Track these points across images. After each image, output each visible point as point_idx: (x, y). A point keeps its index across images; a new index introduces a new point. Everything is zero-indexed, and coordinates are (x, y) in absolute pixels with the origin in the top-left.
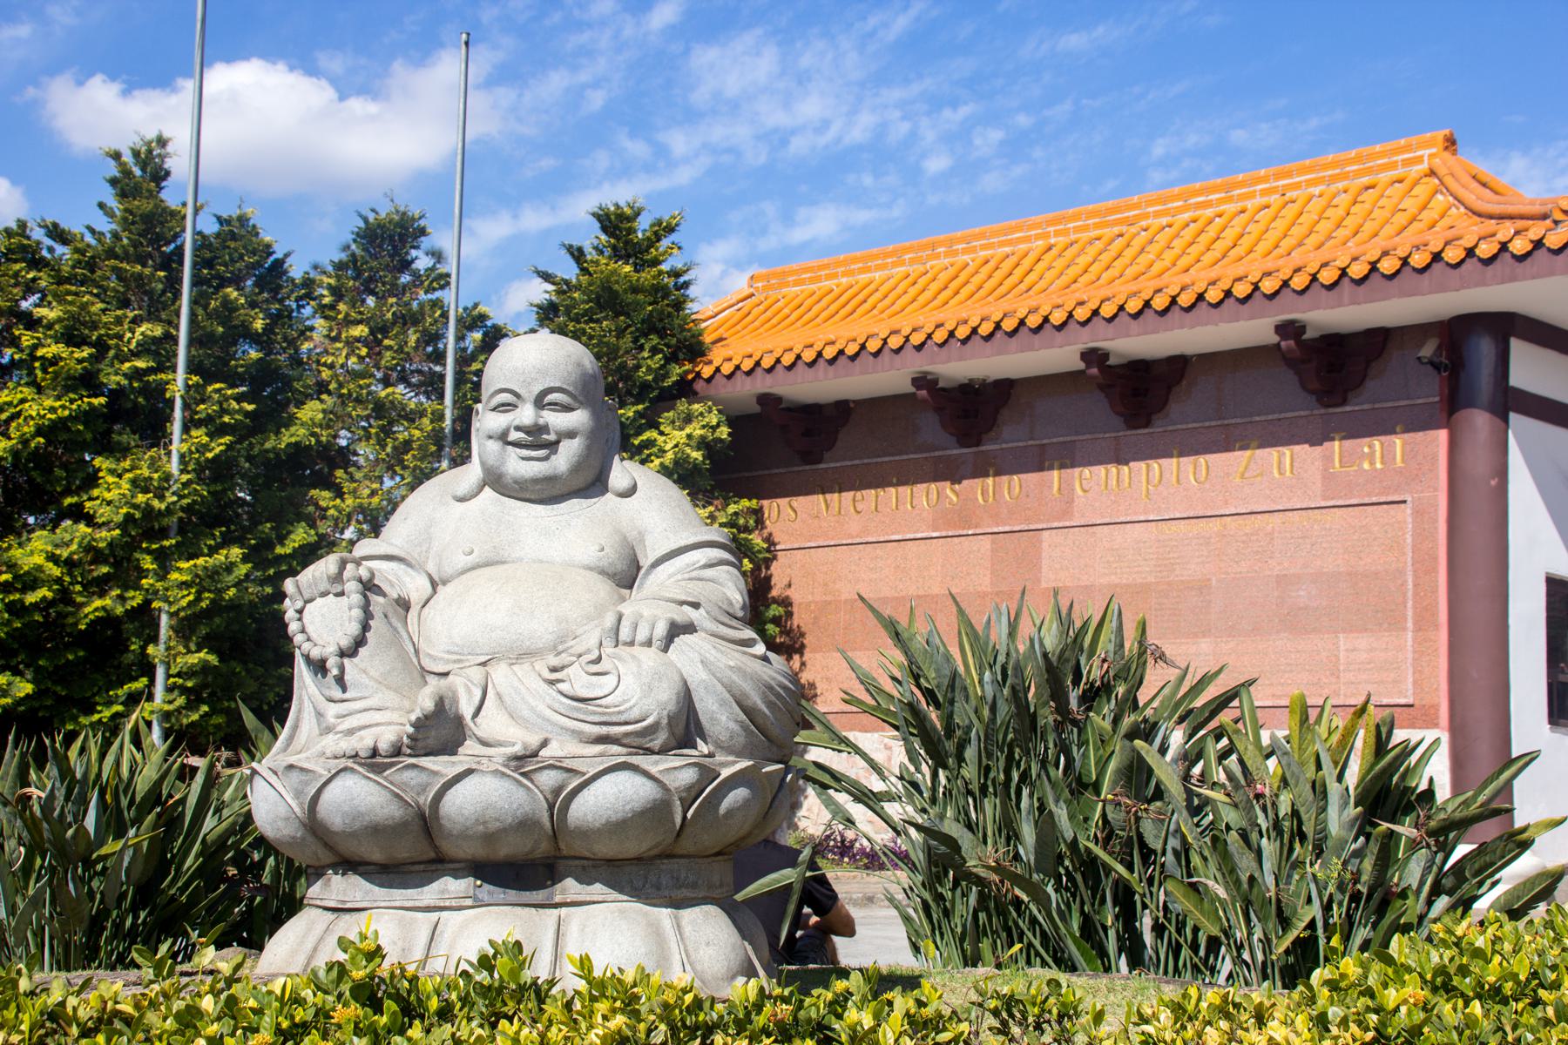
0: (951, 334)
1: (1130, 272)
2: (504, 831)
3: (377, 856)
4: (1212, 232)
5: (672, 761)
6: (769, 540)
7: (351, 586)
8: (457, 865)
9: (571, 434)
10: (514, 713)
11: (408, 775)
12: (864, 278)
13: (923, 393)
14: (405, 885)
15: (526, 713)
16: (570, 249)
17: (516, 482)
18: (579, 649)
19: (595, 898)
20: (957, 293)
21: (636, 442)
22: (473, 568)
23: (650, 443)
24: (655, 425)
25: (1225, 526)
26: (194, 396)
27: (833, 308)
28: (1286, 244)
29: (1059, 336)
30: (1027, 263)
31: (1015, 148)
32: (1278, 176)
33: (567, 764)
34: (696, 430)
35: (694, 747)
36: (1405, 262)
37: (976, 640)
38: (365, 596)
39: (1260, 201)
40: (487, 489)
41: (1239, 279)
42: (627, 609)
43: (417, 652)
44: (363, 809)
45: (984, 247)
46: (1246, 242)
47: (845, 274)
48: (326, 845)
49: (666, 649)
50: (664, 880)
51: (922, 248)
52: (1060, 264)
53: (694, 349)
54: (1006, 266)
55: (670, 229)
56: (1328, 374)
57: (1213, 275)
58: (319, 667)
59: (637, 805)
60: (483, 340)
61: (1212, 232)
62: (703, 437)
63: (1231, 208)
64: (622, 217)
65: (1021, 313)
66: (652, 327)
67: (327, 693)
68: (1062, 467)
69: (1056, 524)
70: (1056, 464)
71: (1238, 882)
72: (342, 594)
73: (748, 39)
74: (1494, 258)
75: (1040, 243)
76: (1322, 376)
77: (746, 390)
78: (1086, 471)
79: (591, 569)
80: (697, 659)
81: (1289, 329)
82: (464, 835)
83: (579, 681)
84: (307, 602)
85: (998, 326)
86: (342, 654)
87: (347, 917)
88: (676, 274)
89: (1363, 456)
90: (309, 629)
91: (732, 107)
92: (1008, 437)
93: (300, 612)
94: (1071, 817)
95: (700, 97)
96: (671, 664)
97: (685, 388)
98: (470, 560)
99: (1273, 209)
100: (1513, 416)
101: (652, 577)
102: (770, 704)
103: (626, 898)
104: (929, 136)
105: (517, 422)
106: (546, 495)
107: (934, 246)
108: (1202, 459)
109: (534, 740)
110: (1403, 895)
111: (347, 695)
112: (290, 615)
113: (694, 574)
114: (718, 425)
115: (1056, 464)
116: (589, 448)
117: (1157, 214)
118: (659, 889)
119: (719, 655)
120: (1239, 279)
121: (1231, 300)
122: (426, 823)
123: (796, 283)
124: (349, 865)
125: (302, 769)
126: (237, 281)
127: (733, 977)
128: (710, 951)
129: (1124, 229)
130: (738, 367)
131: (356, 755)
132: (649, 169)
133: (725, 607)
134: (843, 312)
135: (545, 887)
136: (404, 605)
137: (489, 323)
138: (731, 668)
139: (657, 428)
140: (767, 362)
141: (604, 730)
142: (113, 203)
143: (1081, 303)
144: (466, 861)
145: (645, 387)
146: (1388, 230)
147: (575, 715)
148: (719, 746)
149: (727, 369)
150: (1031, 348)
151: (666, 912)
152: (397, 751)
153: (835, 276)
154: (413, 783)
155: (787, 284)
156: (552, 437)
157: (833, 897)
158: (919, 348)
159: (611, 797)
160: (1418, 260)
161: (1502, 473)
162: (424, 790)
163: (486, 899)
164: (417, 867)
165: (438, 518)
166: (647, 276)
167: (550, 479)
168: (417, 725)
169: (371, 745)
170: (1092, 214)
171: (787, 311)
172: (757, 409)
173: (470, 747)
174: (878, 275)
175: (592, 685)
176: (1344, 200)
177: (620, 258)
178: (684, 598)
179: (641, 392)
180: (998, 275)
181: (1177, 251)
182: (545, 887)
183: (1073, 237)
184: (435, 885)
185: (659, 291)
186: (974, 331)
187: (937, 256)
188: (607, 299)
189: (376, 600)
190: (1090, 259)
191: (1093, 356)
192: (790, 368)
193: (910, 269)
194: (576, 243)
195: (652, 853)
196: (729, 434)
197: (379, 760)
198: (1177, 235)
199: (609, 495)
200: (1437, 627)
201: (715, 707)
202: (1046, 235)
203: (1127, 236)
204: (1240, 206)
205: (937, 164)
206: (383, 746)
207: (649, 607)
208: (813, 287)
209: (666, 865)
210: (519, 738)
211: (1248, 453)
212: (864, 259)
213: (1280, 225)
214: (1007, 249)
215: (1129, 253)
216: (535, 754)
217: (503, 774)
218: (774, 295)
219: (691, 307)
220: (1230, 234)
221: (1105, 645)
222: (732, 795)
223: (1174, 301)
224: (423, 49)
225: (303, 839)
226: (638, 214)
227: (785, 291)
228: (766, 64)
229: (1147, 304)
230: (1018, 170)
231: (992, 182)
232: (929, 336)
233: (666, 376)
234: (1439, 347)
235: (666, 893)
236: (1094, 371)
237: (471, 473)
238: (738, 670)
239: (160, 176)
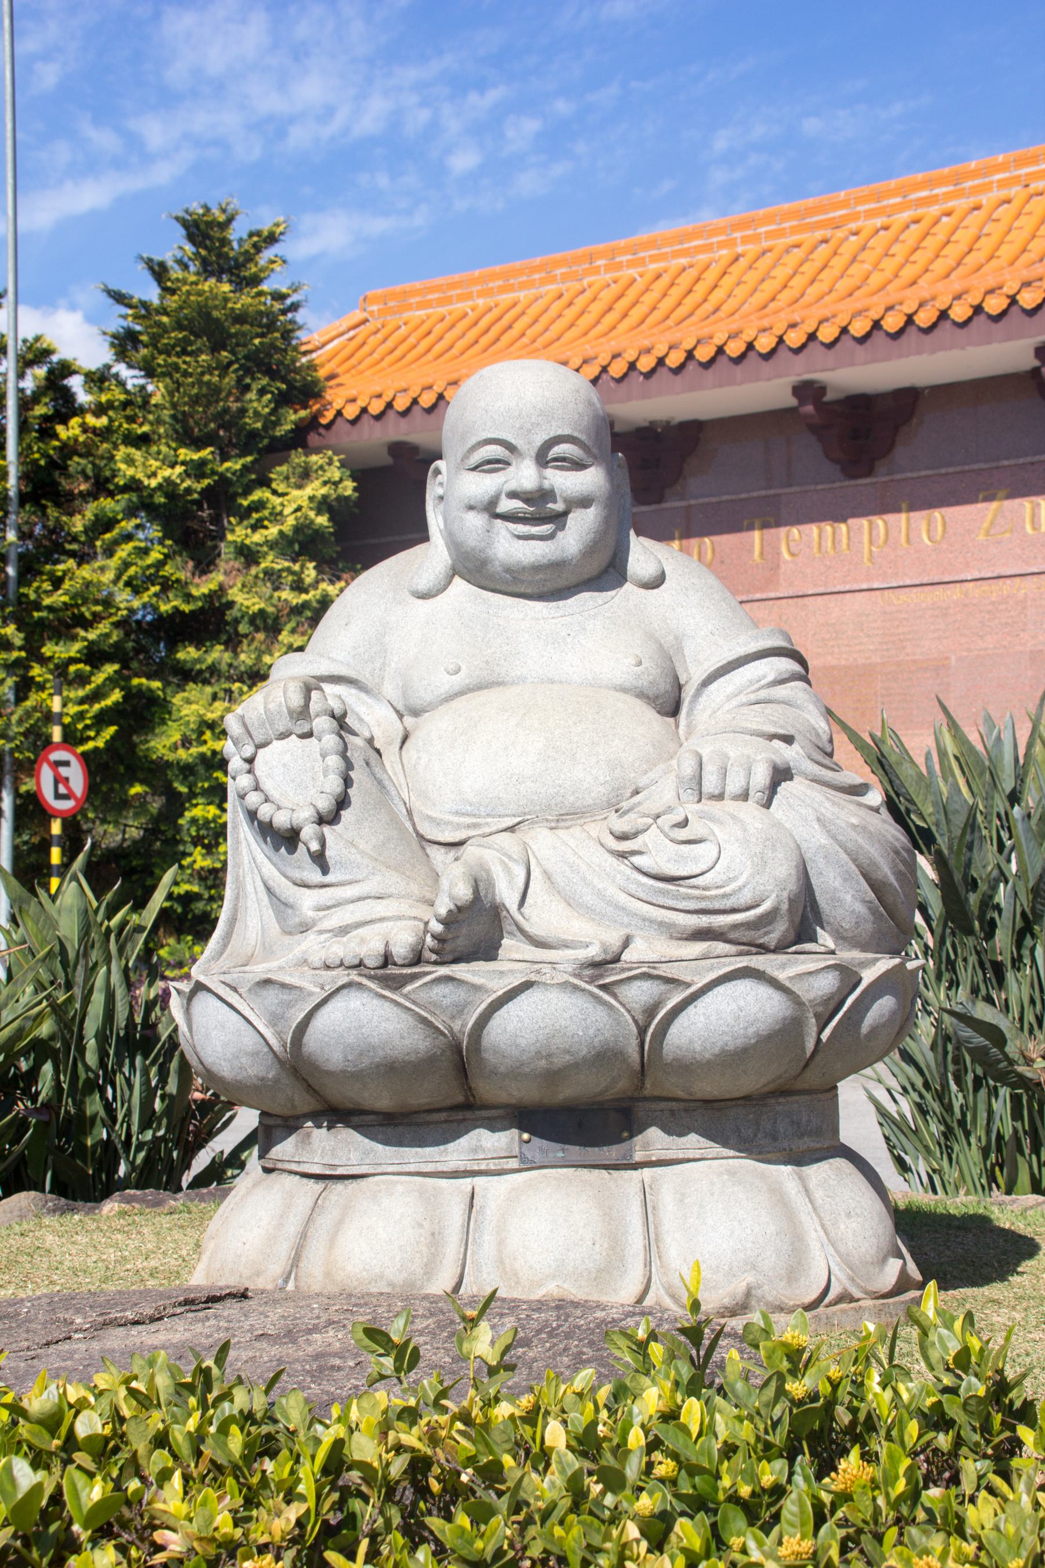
0: (632, 366)
2: (575, 1066)
3: (384, 1102)
7: (322, 723)
8: (493, 1113)
9: (585, 502)
10: (573, 900)
12: (506, 298)
15: (589, 899)
16: (149, 263)
17: (508, 570)
18: (655, 808)
19: (691, 1154)
20: (625, 315)
21: (245, 503)
22: (461, 693)
23: (260, 505)
24: (265, 482)
25: (966, 594)
27: (472, 335)
29: (766, 367)
30: (710, 276)
31: (554, 141)
32: (1020, 162)
33: (664, 970)
34: (315, 488)
35: (813, 939)
38: (341, 737)
40: (457, 580)
41: (990, 292)
43: (409, 813)
44: (375, 1041)
45: (654, 259)
46: (985, 245)
47: (481, 294)
48: (310, 1089)
49: (768, 805)
50: (782, 1126)
51: (577, 260)
52: (752, 277)
53: (303, 390)
55: (272, 239)
58: (287, 839)
60: (47, 379)
62: (325, 497)
63: (962, 204)
67: (297, 875)
68: (765, 526)
69: (758, 596)
70: (757, 523)
72: (309, 735)
77: (374, 438)
78: (795, 531)
79: (624, 690)
80: (812, 817)
82: (515, 1073)
83: (660, 853)
84: (258, 747)
85: (690, 355)
86: (322, 820)
87: (339, 1187)
88: (279, 297)
90: (267, 785)
91: (216, 89)
92: (699, 489)
93: (250, 761)
95: (177, 74)
96: (778, 825)
97: (300, 437)
99: (1016, 204)
101: (703, 699)
103: (732, 1153)
104: (453, 126)
105: (512, 486)
106: (549, 586)
107: (591, 258)
108: (937, 514)
109: (613, 938)
111: (329, 878)
113: (763, 694)
114: (341, 480)
115: (757, 523)
116: (606, 521)
118: (775, 1139)
119: (836, 810)
120: (990, 292)
121: (982, 318)
123: (421, 306)
124: (336, 1114)
125: (283, 986)
127: (884, 1260)
128: (854, 1224)
129: (828, 233)
130: (364, 410)
131: (361, 964)
132: (120, 164)
133: (814, 739)
134: (484, 341)
135: (620, 1140)
137: (55, 358)
138: (854, 827)
139: (269, 486)
140: (401, 404)
141: (704, 921)
143: (793, 326)
144: (507, 1106)
145: (254, 435)
147: (661, 901)
149: (351, 412)
150: (732, 383)
153: (469, 296)
154: (446, 1002)
155: (410, 307)
156: (559, 506)
162: (461, 1012)
163: (538, 1158)
164: (436, 1117)
165: (386, 621)
166: (244, 301)
167: (557, 566)
168: (449, 921)
169: (381, 949)
170: (787, 216)
171: (412, 340)
172: (389, 461)
173: (511, 946)
174: (522, 295)
175: (681, 859)
177: (211, 274)
178: (772, 730)
179: (248, 442)
180: (675, 293)
181: (899, 259)
182: (621, 1141)
183: (765, 244)
184: (464, 1141)
185: (267, 322)
186: (661, 362)
187: (597, 271)
188: (206, 327)
190: (789, 271)
193: (563, 287)
194: (157, 258)
195: (766, 1089)
196: (355, 489)
197: (392, 970)
198: (896, 240)
199: (628, 586)
201: (837, 884)
202: (732, 243)
203: (833, 243)
204: (972, 201)
205: (464, 161)
206: (400, 950)
208: (442, 310)
209: (782, 1105)
210: (595, 938)
211: (994, 505)
212: (505, 275)
214: (684, 261)
215: (838, 263)
216: (617, 959)
217: (576, 988)
218: (393, 321)
219: (302, 335)
220: (963, 237)
222: (876, 1006)
223: (910, 320)
225: (276, 1080)
226: (230, 220)
227: (406, 315)
229: (877, 325)
230: (560, 169)
231: (529, 183)
232: (604, 369)
233: (277, 423)
235: (785, 1144)
236: (809, 409)
237: (430, 559)
238: (893, 836)
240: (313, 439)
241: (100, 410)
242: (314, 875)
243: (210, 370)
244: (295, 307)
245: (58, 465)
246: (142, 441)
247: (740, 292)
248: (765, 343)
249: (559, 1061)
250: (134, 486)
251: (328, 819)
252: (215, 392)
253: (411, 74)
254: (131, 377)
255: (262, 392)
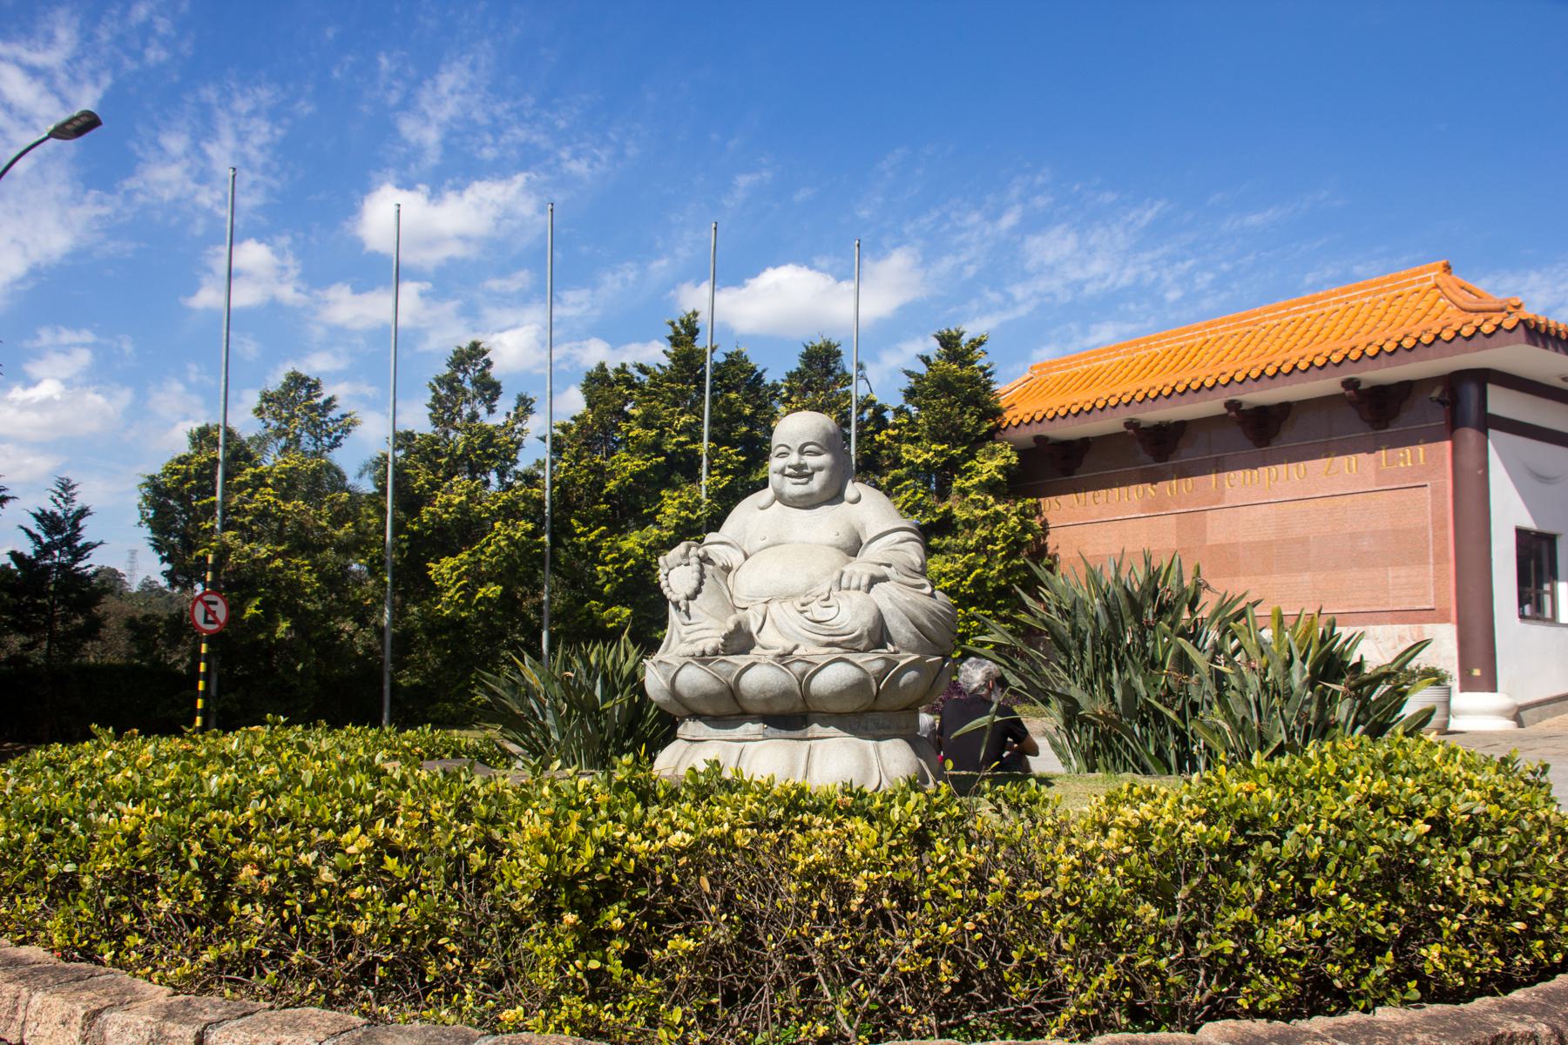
1: (1255, 353)
3: (710, 711)
4: (1304, 327)
5: (870, 656)
6: (1045, 524)
7: (694, 560)
9: (820, 469)
11: (721, 666)
13: (1131, 431)
14: (726, 728)
16: (921, 357)
23: (970, 469)
24: (974, 458)
26: (713, 454)
28: (1348, 332)
32: (1343, 292)
36: (1418, 340)
37: (1093, 577)
39: (1333, 307)
42: (848, 569)
46: (1323, 334)
50: (870, 725)
53: (997, 413)
54: (1181, 354)
55: (981, 343)
56: (1373, 410)
57: (1302, 353)
59: (849, 682)
61: (1304, 327)
64: (951, 337)
65: (1188, 381)
66: (973, 400)
71: (1235, 721)
73: (1059, 230)
74: (1472, 336)
75: (1201, 339)
76: (1373, 410)
77: (1027, 434)
78: (1232, 474)
81: (1350, 384)
82: (753, 700)
83: (817, 611)
85: (1174, 389)
86: (688, 598)
87: (696, 745)
88: (982, 369)
89: (1400, 459)
91: (1051, 270)
92: (1185, 456)
94: (1145, 684)
95: (1030, 265)
97: (991, 435)
98: (765, 542)
100: (1491, 432)
102: (932, 622)
109: (790, 646)
110: (1336, 726)
112: (662, 577)
117: (1271, 318)
122: (732, 692)
124: (697, 716)
126: (736, 388)
132: (1002, 308)
136: (727, 569)
140: (1038, 418)
141: (831, 639)
142: (671, 350)
145: (968, 435)
146: (1410, 321)
148: (902, 647)
149: (1015, 422)
151: (871, 743)
152: (716, 652)
157: (1026, 732)
158: (1127, 404)
159: (833, 677)
160: (1426, 339)
161: (1485, 465)
166: (966, 372)
167: (809, 495)
168: (726, 637)
173: (757, 650)
174: (1105, 363)
176: (1383, 305)
185: (973, 381)
189: (708, 568)
191: (1232, 405)
192: (1052, 420)
200: (1448, 561)
206: (708, 650)
207: (860, 569)
209: (871, 716)
213: (1344, 322)
215: (1254, 343)
218: (1044, 377)
220: (1315, 328)
221: (1173, 580)
223: (1279, 370)
224: (879, 251)
228: (1070, 242)
229: (1263, 372)
230: (1223, 296)
234: (1443, 392)
238: (912, 602)
239: (694, 333)
240: (997, 436)
241: (895, 427)
242: (686, 620)
243: (946, 406)
244: (991, 374)
245: (876, 453)
246: (912, 441)
247: (1207, 357)
248: (1209, 383)
249: (769, 695)
250: (910, 463)
251: (693, 596)
252: (948, 416)
253: (1148, 256)
254: (914, 410)
255: (972, 414)
